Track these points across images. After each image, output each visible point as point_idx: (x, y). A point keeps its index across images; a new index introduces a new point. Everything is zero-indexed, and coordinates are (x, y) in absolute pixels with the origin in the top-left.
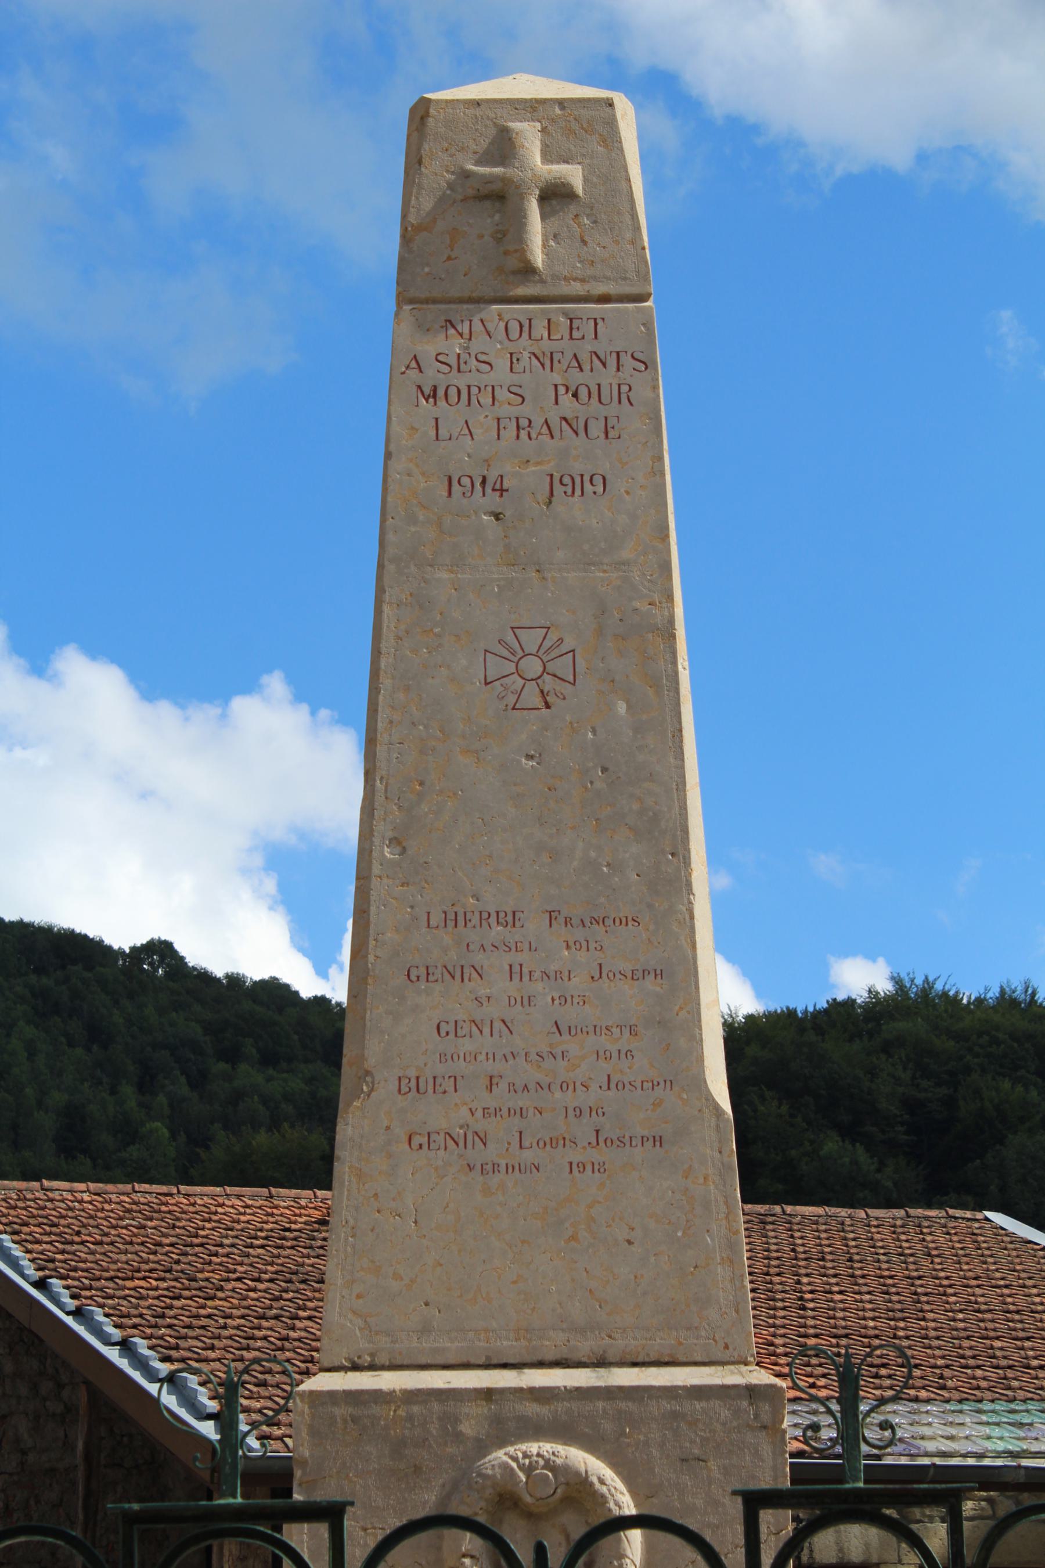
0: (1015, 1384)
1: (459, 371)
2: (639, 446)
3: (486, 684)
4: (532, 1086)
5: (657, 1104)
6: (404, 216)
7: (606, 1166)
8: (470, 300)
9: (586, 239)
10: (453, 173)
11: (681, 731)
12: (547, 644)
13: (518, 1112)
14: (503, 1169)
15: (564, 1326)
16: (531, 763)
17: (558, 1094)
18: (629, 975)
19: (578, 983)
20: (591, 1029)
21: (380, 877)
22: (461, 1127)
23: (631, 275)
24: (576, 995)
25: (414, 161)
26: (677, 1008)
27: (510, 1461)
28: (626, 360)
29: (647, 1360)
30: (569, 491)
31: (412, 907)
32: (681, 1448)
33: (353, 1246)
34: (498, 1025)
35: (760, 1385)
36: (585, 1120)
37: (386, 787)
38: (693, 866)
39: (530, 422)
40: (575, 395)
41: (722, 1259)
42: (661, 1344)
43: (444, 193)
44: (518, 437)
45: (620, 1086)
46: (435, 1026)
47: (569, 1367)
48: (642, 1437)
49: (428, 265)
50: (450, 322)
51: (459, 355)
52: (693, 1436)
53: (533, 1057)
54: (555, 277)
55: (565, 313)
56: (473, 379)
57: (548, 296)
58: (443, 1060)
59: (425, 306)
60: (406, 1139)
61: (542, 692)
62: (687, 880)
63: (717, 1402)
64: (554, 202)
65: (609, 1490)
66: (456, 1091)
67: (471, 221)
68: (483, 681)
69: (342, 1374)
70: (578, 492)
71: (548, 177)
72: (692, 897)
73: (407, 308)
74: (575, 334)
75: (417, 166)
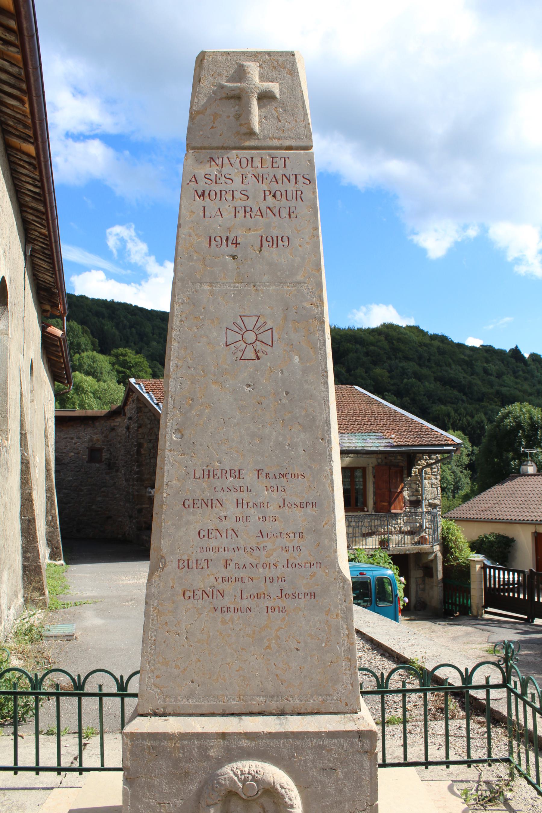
0: (362, 429)
1: (216, 183)
2: (306, 222)
3: (227, 346)
4: (247, 565)
5: (313, 575)
6: (191, 107)
7: (286, 609)
8: (223, 148)
9: (281, 118)
10: (215, 86)
11: (327, 372)
12: (258, 325)
13: (240, 579)
14: (232, 610)
15: (263, 694)
16: (249, 389)
17: (261, 570)
18: (299, 505)
19: (272, 510)
20: (279, 534)
21: (170, 450)
22: (210, 587)
23: (303, 136)
24: (271, 515)
25: (197, 80)
26: (324, 523)
27: (234, 776)
28: (300, 179)
29: (306, 712)
30: (271, 245)
31: (186, 467)
32: (323, 763)
33: (155, 651)
34: (230, 532)
35: (365, 731)
36: (275, 583)
37: (174, 401)
38: (333, 445)
39: (251, 209)
40: (274, 196)
41: (345, 658)
42: (313, 703)
43: (211, 96)
44: (245, 217)
45: (294, 566)
46: (198, 532)
47: (265, 715)
48: (303, 758)
49: (202, 130)
50: (212, 158)
51: (216, 175)
52: (329, 757)
53: (248, 549)
54: (265, 137)
55: (270, 155)
56: (223, 187)
57: (261, 146)
58: (202, 551)
59: (200, 151)
60: (182, 593)
61: (255, 350)
62: (329, 454)
63: (342, 740)
64: (265, 101)
65: (286, 792)
66: (208, 568)
67: (224, 109)
68: (225, 345)
69: (149, 718)
70: (275, 245)
71: (262, 88)
72: (332, 462)
73: (191, 151)
74: (275, 165)
75: (198, 83)
